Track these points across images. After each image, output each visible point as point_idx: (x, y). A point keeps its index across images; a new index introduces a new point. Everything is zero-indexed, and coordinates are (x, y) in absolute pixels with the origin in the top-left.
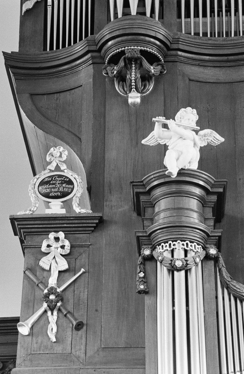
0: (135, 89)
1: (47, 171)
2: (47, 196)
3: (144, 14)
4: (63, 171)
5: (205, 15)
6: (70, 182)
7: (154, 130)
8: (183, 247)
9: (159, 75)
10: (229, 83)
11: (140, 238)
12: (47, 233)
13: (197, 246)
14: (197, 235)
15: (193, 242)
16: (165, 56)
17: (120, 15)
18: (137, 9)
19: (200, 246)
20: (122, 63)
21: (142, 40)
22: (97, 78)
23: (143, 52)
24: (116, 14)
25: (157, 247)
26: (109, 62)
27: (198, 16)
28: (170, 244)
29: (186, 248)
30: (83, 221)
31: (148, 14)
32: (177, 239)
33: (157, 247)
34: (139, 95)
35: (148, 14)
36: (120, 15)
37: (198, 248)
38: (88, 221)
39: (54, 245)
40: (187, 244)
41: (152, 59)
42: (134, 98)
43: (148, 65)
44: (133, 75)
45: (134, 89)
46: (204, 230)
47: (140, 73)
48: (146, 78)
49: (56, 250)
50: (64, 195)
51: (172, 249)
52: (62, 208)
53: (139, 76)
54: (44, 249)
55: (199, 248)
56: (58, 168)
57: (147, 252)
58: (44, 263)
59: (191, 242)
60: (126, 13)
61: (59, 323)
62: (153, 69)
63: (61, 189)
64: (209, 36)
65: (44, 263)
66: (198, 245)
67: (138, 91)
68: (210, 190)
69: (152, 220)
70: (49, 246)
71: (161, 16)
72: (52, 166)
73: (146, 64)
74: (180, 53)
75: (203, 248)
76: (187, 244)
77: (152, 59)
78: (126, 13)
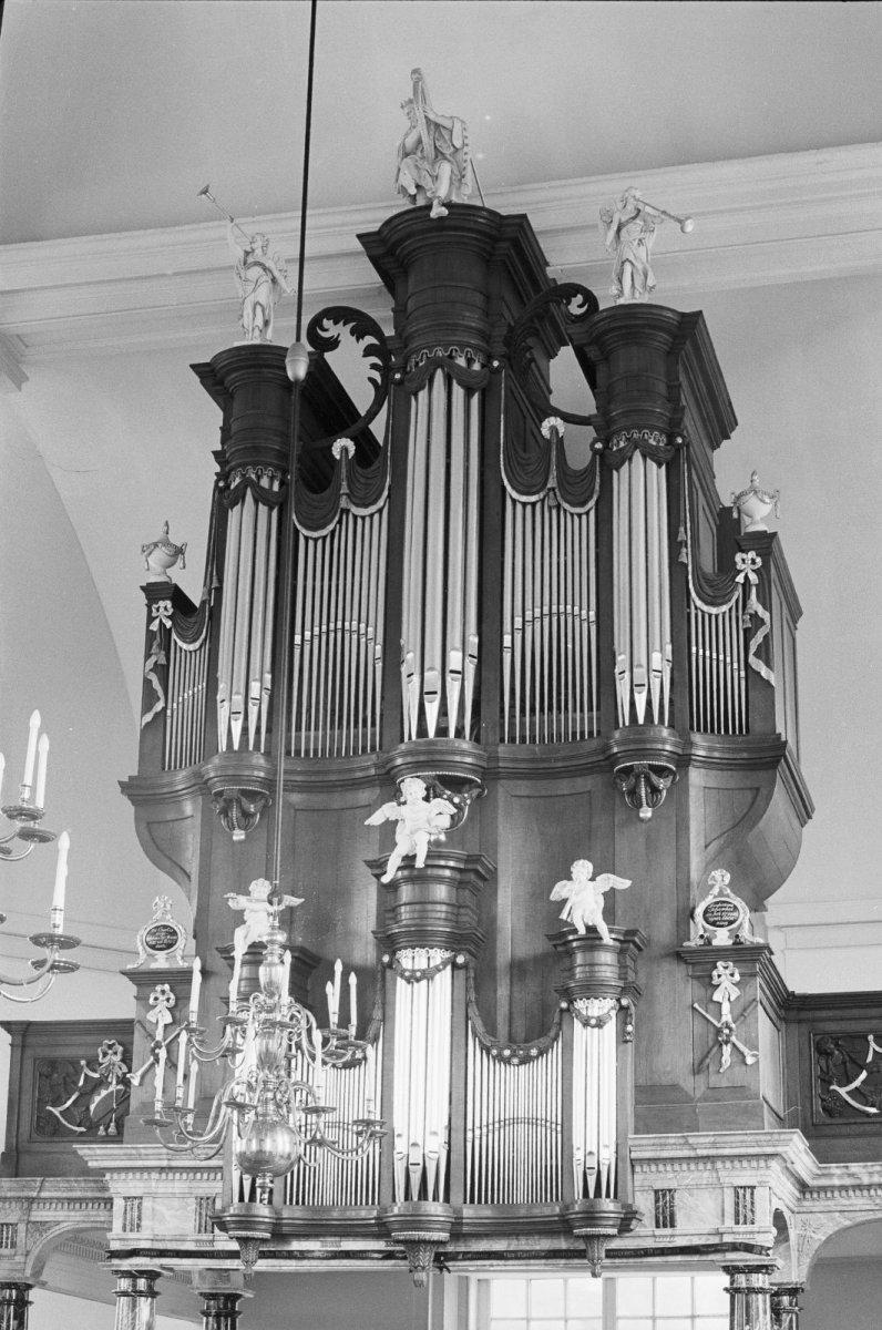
1: (710, 897)
2: (153, 947)
4: (728, 896)
5: (316, 729)
12: (155, 984)
22: (206, 813)
24: (410, 738)
26: (619, 771)
27: (310, 730)
36: (414, 738)
39: (161, 998)
42: (239, 835)
49: (162, 1005)
50: (170, 946)
54: (151, 1001)
56: (721, 894)
58: (717, 997)
60: (422, 732)
63: (166, 941)
64: (303, 755)
65: (717, 997)
70: (156, 999)
72: (716, 891)
78: (422, 732)
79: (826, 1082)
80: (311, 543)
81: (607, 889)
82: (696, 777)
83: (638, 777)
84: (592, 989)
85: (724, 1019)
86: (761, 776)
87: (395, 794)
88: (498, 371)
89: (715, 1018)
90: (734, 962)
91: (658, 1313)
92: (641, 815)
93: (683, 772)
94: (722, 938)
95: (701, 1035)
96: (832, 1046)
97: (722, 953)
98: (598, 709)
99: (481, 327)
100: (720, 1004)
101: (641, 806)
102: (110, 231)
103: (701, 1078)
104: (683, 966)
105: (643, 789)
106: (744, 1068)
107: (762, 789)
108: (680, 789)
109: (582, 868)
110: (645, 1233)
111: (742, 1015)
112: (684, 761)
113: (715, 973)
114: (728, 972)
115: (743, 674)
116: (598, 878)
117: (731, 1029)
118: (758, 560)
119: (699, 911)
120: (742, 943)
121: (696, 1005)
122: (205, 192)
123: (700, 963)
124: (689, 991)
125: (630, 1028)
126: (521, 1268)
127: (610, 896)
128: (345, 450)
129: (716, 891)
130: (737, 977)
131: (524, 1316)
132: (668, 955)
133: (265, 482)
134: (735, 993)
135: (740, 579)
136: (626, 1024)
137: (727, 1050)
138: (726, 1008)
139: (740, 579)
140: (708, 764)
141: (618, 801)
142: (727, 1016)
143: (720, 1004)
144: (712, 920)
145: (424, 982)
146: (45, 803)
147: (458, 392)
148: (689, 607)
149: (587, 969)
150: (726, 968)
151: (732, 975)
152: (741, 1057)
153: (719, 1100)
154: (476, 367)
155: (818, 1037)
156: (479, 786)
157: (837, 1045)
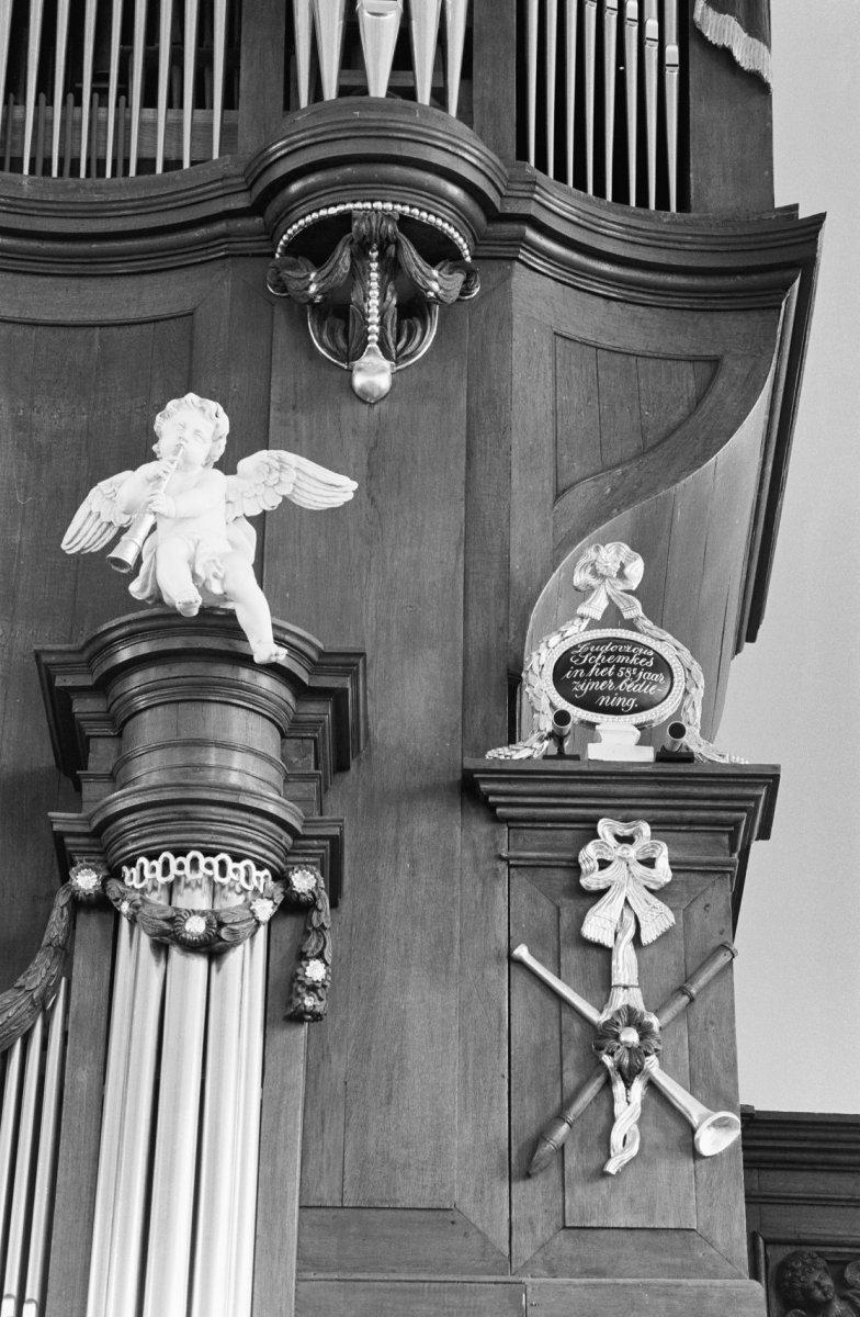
0: (378, 343)
3: (410, 93)
4: (631, 625)
6: (661, 665)
7: (134, 469)
8: (210, 873)
9: (458, 300)
10: (155, 321)
11: (68, 840)
13: (255, 873)
14: (260, 839)
15: (213, 853)
16: (477, 239)
17: (330, 91)
18: (391, 76)
19: (266, 872)
20: (343, 259)
21: (419, 187)
23: (405, 222)
25: (125, 869)
26: (291, 248)
28: (166, 864)
29: (217, 878)
30: (613, 788)
31: (424, 96)
32: (219, 847)
33: (125, 869)
34: (387, 364)
35: (424, 96)
36: (330, 91)
37: (258, 878)
38: (687, 790)
40: (222, 864)
41: (438, 250)
43: (420, 263)
44: (374, 301)
45: (375, 346)
46: (287, 823)
47: (396, 291)
48: (413, 308)
51: (171, 878)
52: (641, 743)
53: (394, 302)
55: (261, 878)
56: (613, 616)
57: (86, 881)
58: (598, 925)
59: (179, 853)
61: (603, 1119)
62: (438, 283)
65: (598, 925)
66: (260, 867)
67: (387, 356)
68: (306, 680)
69: (116, 778)
71: (465, 114)
72: (596, 607)
73: (411, 256)
74: (531, 235)
75: (275, 878)
76: (222, 864)
77: (438, 250)
78: (354, 88)
81: (271, 502)
82: (536, 298)
83: (360, 253)
84: (187, 819)
85: (620, 999)
86: (728, 331)
89: (586, 995)
90: (659, 827)
92: (359, 380)
93: (494, 277)
94: (617, 742)
95: (540, 1050)
96: (828, 1282)
97: (616, 790)
98: (230, 102)
100: (606, 952)
103: (534, 1195)
104: (481, 829)
105: (374, 293)
106: (688, 1166)
107: (727, 360)
108: (475, 338)
109: (192, 424)
111: (682, 990)
112: (500, 231)
113: (590, 853)
114: (632, 852)
115: (672, 51)
116: (245, 465)
117: (645, 1031)
119: (541, 660)
120: (688, 758)
121: (522, 952)
123: (537, 819)
124: (504, 906)
125: (315, 971)
126: (571, 217)
127: (275, 531)
130: (663, 873)
132: (429, 791)
134: (657, 920)
136: (302, 957)
137: (629, 1103)
138: (625, 966)
140: (582, 266)
141: (282, 336)
142: (627, 996)
143: (606, 952)
144: (584, 688)
149: (178, 757)
150: (629, 840)
151: (649, 863)
152: (678, 1131)
153: (599, 1273)
155: (780, 1254)
157: (841, 1282)
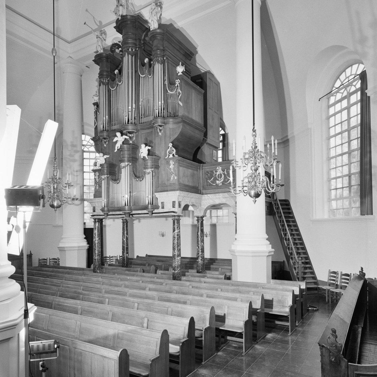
6: (173, 150)
72: (170, 147)
79: (207, 180)
80: (113, 91)
87: (116, 136)
88: (138, 51)
91: (218, 216)
99: (133, 42)
101: (159, 133)
102: (85, 36)
110: (160, 210)
118: (180, 81)
122: (85, 24)
128: (117, 72)
129: (170, 147)
130: (174, 163)
131: (216, 216)
133: (104, 81)
135: (176, 85)
139: (176, 85)
145: (124, 169)
146: (219, 144)
147: (130, 56)
148: (167, 92)
154: (134, 50)
156: (136, 132)
